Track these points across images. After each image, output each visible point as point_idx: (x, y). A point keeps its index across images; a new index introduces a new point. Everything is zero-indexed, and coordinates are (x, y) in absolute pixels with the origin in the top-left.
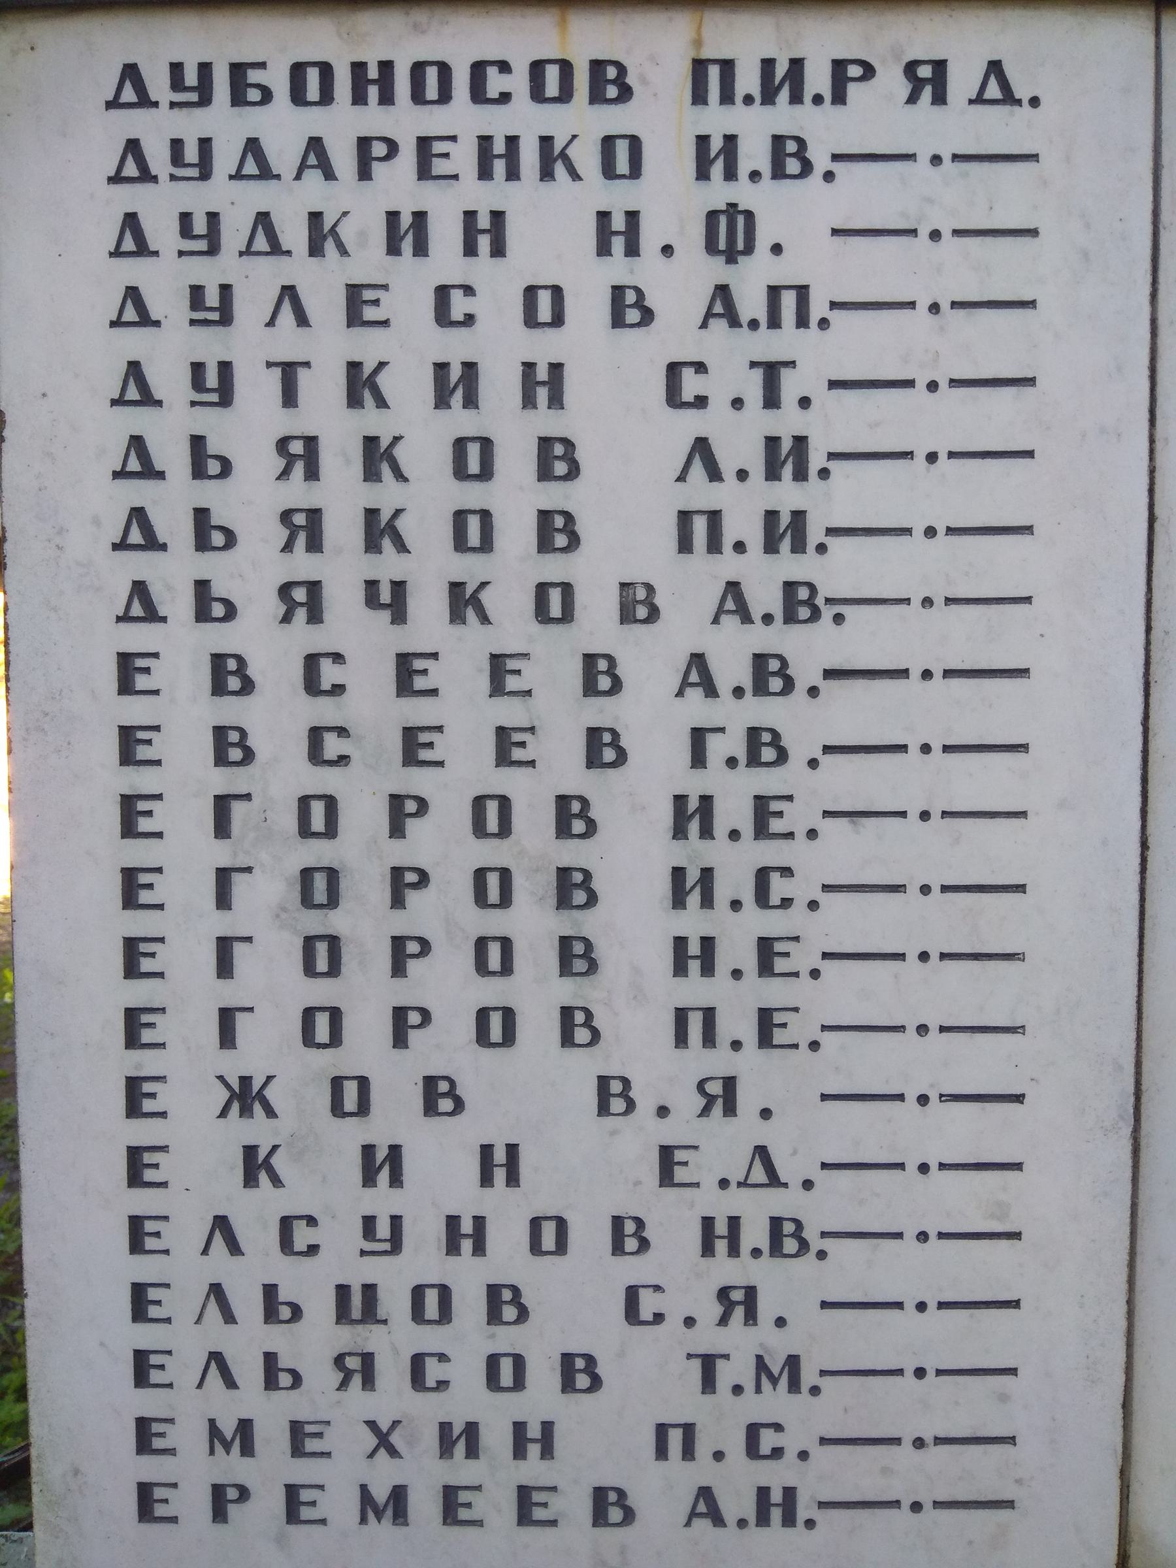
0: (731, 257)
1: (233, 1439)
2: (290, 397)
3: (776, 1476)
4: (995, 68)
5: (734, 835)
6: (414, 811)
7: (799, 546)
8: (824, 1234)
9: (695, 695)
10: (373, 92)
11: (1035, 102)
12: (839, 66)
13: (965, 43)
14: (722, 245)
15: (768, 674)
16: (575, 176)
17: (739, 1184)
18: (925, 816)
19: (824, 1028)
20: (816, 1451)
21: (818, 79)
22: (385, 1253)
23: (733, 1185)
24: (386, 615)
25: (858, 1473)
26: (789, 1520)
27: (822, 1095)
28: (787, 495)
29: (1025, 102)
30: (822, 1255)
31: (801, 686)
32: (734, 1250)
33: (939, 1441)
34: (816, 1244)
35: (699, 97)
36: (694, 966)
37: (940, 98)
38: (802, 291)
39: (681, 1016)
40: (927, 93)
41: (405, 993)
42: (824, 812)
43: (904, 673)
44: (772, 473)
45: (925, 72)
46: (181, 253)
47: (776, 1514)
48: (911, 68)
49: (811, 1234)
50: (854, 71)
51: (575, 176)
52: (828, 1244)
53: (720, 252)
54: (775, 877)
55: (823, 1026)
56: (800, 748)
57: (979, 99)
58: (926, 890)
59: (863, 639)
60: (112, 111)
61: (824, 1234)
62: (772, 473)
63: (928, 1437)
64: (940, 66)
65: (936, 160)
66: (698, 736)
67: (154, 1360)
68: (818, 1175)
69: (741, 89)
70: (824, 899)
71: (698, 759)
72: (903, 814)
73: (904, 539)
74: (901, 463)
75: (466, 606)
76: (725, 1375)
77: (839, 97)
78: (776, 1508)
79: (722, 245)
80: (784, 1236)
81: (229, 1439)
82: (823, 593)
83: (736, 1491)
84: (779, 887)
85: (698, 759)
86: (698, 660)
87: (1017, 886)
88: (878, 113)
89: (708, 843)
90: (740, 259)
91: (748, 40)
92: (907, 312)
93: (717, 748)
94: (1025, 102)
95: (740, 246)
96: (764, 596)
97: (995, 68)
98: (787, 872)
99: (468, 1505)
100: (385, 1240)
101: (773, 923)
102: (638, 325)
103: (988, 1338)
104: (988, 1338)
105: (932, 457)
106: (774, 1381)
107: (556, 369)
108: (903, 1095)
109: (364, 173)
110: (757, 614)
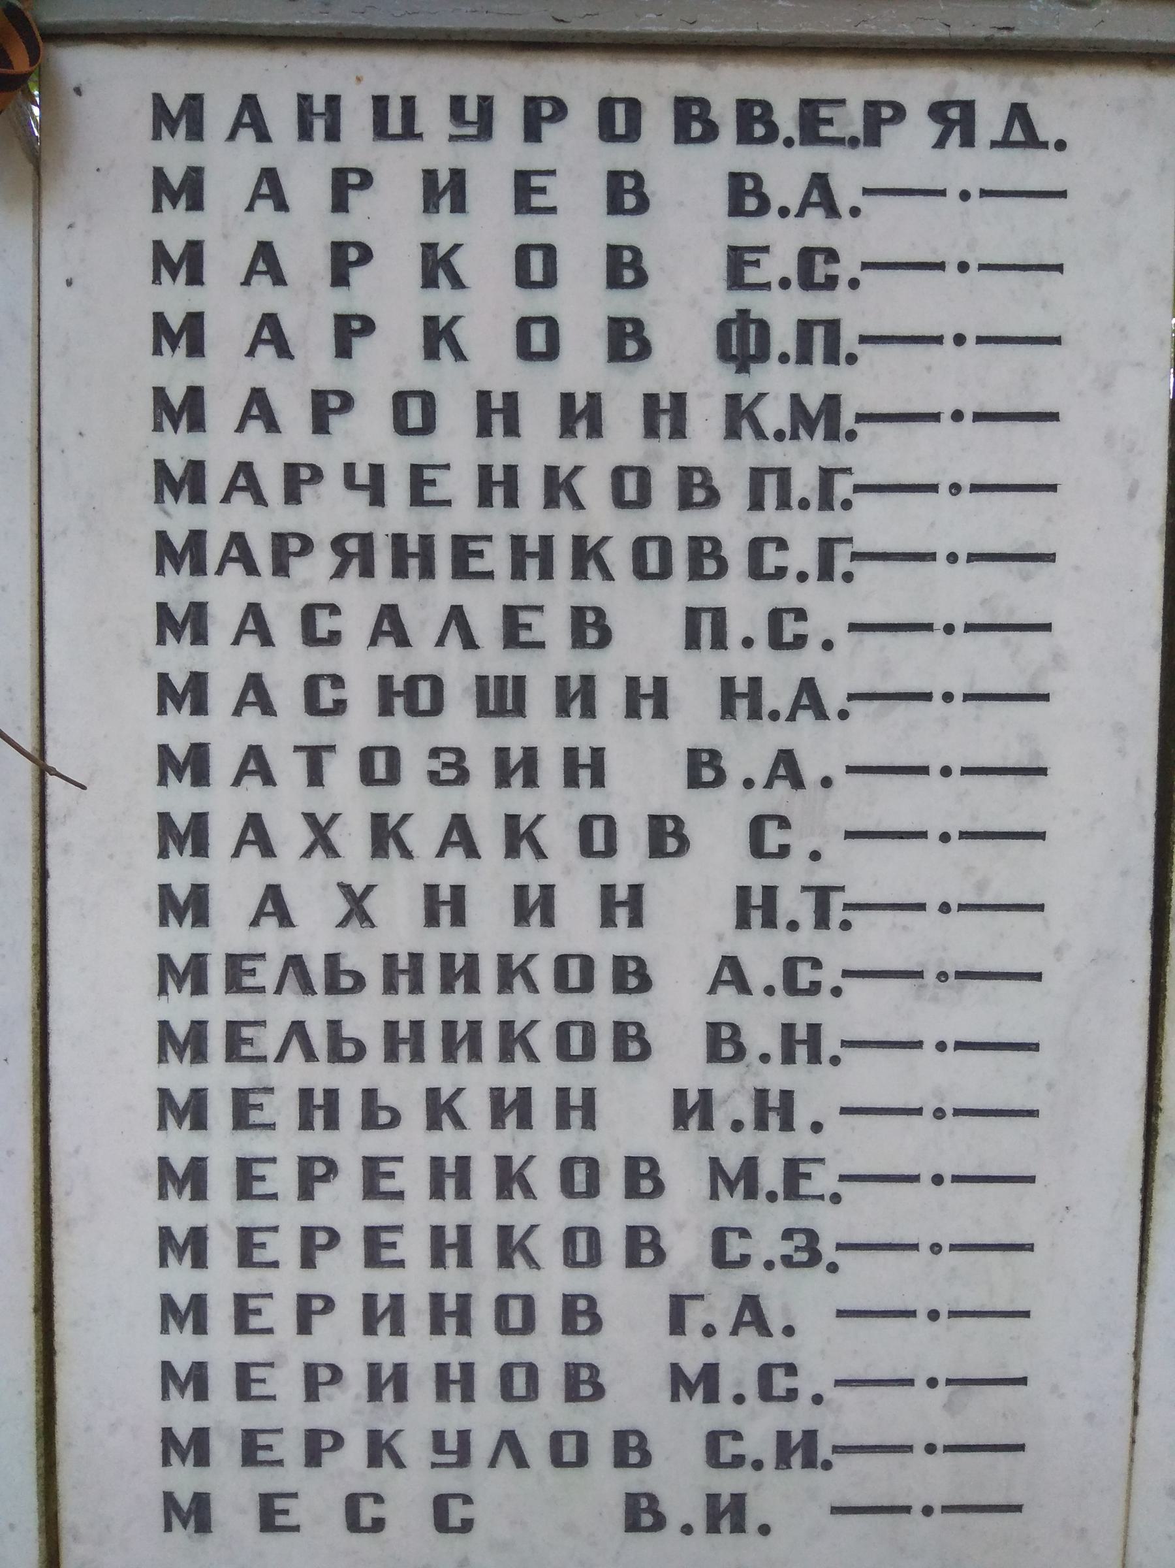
1: (187, 1313)
2: (315, 777)
4: (1019, 112)
5: (737, 1126)
8: (840, 1247)
10: (413, 565)
11: (1061, 145)
13: (990, 92)
14: (753, 328)
15: (782, 630)
16: (607, 575)
20: (832, 1395)
21: (852, 121)
22: (257, 1365)
24: (364, 497)
26: (815, 1057)
28: (801, 1011)
29: (1051, 146)
37: (968, 141)
38: (833, 327)
40: (956, 133)
41: (347, 228)
42: (841, 1176)
43: (924, 770)
45: (954, 113)
46: (434, 1465)
47: (802, 1052)
50: (887, 113)
51: (607, 575)
53: (754, 321)
58: (936, 1249)
60: (244, 1201)
63: (965, 484)
64: (968, 107)
65: (965, 195)
67: (253, 1304)
71: (677, 1325)
73: (920, 779)
76: (695, 1315)
77: (873, 138)
79: (753, 328)
81: (176, 261)
86: (731, 962)
87: (1016, 1506)
88: (910, 149)
92: (936, 273)
94: (1051, 146)
96: (762, 1036)
97: (1019, 112)
101: (819, 306)
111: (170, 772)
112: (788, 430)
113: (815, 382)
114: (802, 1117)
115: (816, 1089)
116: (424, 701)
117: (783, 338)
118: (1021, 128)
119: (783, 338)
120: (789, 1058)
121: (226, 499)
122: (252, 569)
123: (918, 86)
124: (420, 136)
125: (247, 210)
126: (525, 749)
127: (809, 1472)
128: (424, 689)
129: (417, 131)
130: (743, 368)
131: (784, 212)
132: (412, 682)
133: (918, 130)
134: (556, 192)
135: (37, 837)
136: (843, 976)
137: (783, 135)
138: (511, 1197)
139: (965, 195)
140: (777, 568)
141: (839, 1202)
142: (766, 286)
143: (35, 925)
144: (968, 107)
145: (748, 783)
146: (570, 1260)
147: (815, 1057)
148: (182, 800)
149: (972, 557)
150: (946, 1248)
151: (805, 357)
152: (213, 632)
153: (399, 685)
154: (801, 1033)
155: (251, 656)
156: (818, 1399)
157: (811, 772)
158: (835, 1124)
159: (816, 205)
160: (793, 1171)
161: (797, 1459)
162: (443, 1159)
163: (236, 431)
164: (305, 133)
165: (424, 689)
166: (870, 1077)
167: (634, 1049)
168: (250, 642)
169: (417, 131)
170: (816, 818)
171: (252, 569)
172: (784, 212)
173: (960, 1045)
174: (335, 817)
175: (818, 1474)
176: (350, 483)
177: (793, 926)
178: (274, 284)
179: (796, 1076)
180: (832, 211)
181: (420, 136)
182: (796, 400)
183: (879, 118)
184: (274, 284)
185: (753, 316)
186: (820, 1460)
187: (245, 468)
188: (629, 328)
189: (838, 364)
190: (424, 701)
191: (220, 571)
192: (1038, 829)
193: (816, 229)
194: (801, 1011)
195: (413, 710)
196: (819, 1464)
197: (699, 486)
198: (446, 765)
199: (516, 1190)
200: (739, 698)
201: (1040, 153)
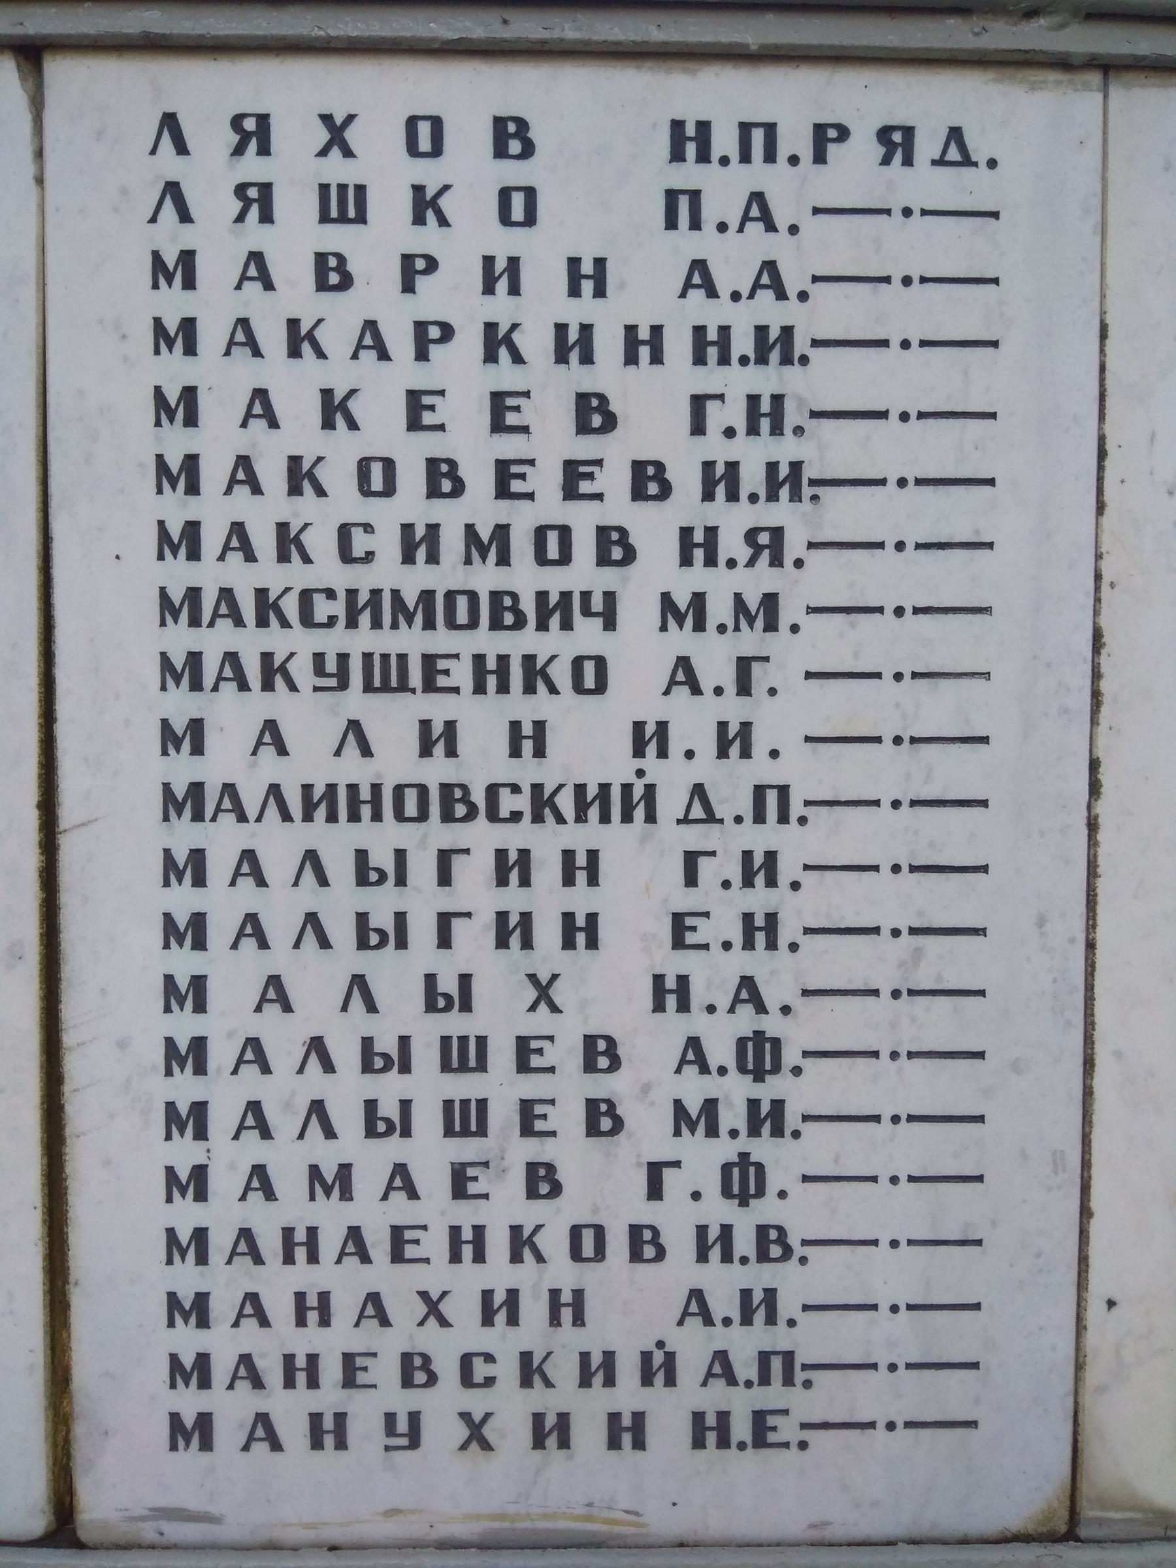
0: (759, 1035)
4: (955, 134)
8: (805, 1242)
9: (697, 295)
13: (929, 101)
14: (736, 1189)
16: (553, 690)
18: (891, 1426)
19: (807, 867)
30: (803, 1445)
33: (911, 1118)
34: (799, 1250)
35: (671, 223)
37: (908, 161)
38: (783, 791)
39: (672, 196)
40: (898, 157)
43: (883, 415)
44: (748, 881)
46: (316, 689)
48: (884, 134)
49: (794, 1241)
50: (832, 133)
52: (809, 1251)
55: (803, 1116)
57: (685, 820)
61: (805, 1242)
62: (749, 944)
64: (908, 132)
68: (797, 1002)
69: (735, 1438)
71: (691, 880)
72: (874, 1179)
73: (883, 350)
74: (872, 351)
75: (524, 1245)
77: (820, 157)
80: (772, 1243)
82: (808, 473)
85: (691, 880)
88: (855, 169)
90: (768, 1078)
92: (872, 874)
95: (736, 1171)
97: (955, 134)
99: (544, 1117)
105: (894, 1180)
106: (751, 621)
107: (592, 918)
109: (422, 355)
110: (707, 685)
111: (172, 939)
112: (731, 625)
113: (765, 380)
114: (761, 744)
115: (779, 1158)
118: (957, 149)
122: (239, 622)
123: (865, 99)
126: (508, 1291)
127: (787, 369)
131: (736, 296)
133: (862, 148)
135: (40, 499)
136: (803, 1057)
139: (894, 1309)
140: (754, 1032)
143: (38, 406)
144: (908, 132)
148: (183, 900)
149: (921, 415)
150: (911, 482)
151: (762, 359)
152: (213, 1129)
155: (247, 896)
159: (765, 287)
161: (775, 356)
164: (289, 1383)
167: (617, 553)
168: (246, 884)
170: (779, 719)
171: (239, 622)
172: (736, 296)
173: (919, 482)
174: (444, 1294)
175: (795, 370)
178: (253, 493)
179: (763, 1149)
182: (738, 598)
183: (826, 137)
184: (253, 493)
185: (753, 1159)
186: (797, 355)
187: (246, 1360)
188: (595, 403)
189: (783, 1136)
191: (211, 624)
194: (759, 900)
196: (796, 362)
201: (971, 170)
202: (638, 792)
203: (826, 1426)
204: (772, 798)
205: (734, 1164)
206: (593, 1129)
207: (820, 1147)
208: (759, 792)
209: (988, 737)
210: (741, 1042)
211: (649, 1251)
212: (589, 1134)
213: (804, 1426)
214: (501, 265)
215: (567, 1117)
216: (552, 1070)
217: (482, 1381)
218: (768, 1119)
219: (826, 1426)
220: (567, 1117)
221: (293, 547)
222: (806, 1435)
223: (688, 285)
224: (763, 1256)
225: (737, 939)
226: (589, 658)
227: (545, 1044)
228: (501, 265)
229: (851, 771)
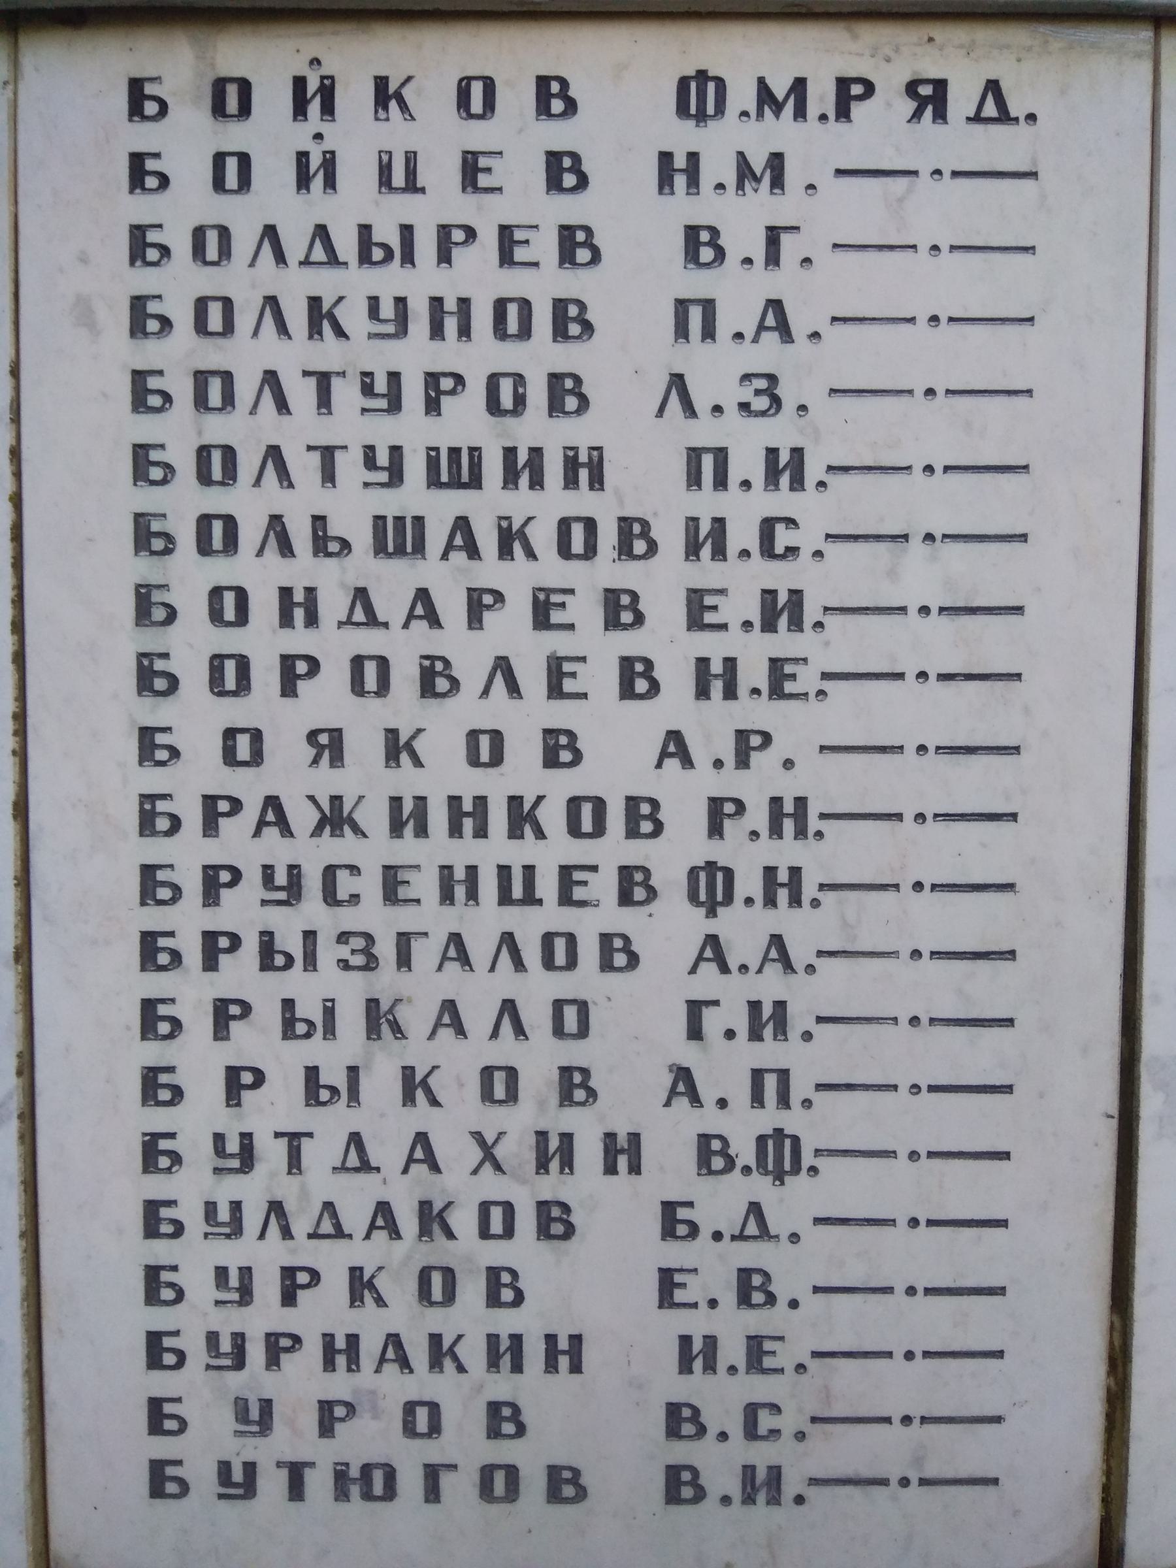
3: (782, 432)
4: (993, 87)
6: (337, 550)
7: (796, 624)
8: (823, 816)
11: (1031, 117)
12: (843, 84)
13: (962, 58)
14: (720, 876)
17: (734, 1238)
21: (821, 96)
23: (727, 1238)
25: (848, 1322)
26: (795, 900)
27: (814, 1287)
29: (1022, 119)
31: (789, 405)
32: (730, 693)
36: (680, 162)
37: (940, 115)
42: (823, 674)
43: (891, 1154)
47: (783, 895)
48: (911, 88)
54: (780, 528)
56: (799, 1019)
57: (977, 118)
59: (843, 1187)
64: (940, 85)
66: (695, 1008)
68: (808, 1428)
70: (818, 963)
77: (843, 112)
78: (760, 1486)
79: (720, 876)
83: (720, 1466)
84: (783, 538)
85: (695, 1032)
89: (721, 495)
91: (747, 55)
92: (897, 618)
93: (713, 1022)
94: (1022, 119)
98: (791, 522)
100: (232, 1156)
102: (632, 625)
103: (991, 644)
104: (991, 644)
108: (901, 815)
110: (733, 964)
113: (786, 852)
116: (378, 1489)
117: (749, 883)
118: (995, 107)
119: (749, 883)
120: (770, 901)
121: (445, 556)
123: (893, 55)
124: (422, 190)
125: (689, 973)
128: (378, 1477)
129: (419, 186)
130: (712, 913)
131: (744, 968)
132: (367, 1469)
134: (499, 173)
137: (739, 1163)
138: (522, 837)
141: (809, 1107)
142: (723, 627)
144: (940, 85)
145: (739, 336)
146: (574, 830)
147: (795, 900)
153: (354, 1472)
154: (783, 876)
156: (794, 1304)
157: (799, 324)
158: (811, 1304)
160: (756, 1348)
162: (459, 798)
163: (254, 486)
165: (378, 1477)
166: (843, 1187)
169: (419, 186)
173: (932, 1089)
176: (368, 389)
177: (723, 1436)
180: (788, 965)
181: (422, 190)
183: (849, 94)
185: (770, 1178)
190: (378, 1489)
192: (991, 1475)
193: (766, 354)
195: (368, 1496)
197: (706, 244)
198: (758, 392)
199: (528, 830)
200: (711, 1153)
202: (313, 85)
203: (846, 469)
204: (771, 1082)
205: (722, 904)
206: (627, 692)
207: (847, 714)
208: (757, 1075)
209: (1006, 1221)
210: (761, 1140)
211: (620, 960)
212: (623, 697)
213: (826, 676)
214: (318, 183)
215: (598, 676)
216: (571, 627)
217: (347, 898)
218: (780, 1156)
219: (846, 469)
220: (598, 676)
221: (366, 1292)
222: (827, 686)
223: (664, 755)
224: (769, 626)
225: (735, 1491)
226: (561, 968)
227: (566, 598)
228: (318, 183)
229: (848, 1322)
